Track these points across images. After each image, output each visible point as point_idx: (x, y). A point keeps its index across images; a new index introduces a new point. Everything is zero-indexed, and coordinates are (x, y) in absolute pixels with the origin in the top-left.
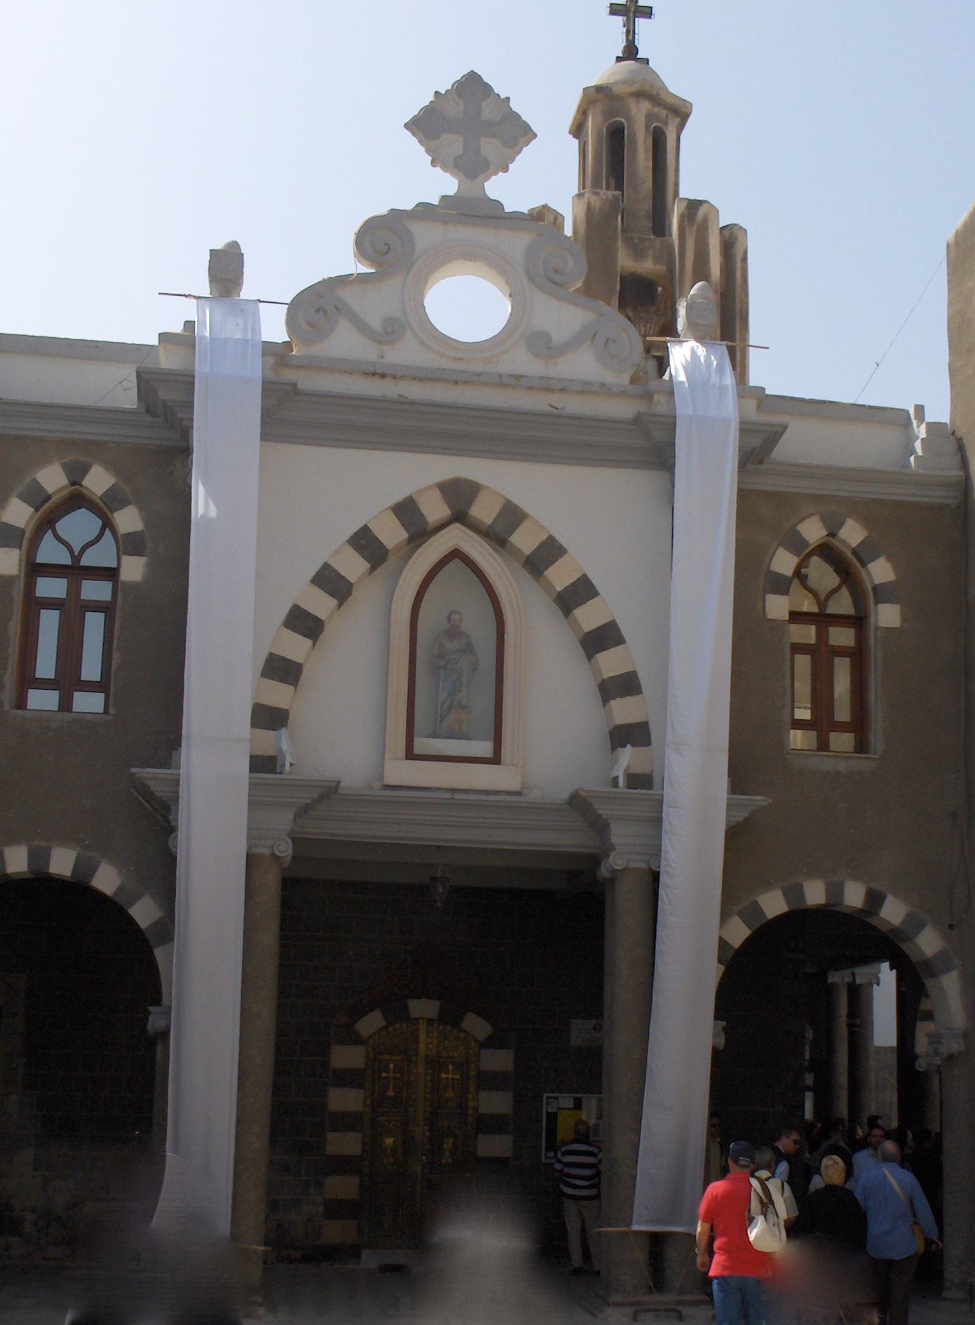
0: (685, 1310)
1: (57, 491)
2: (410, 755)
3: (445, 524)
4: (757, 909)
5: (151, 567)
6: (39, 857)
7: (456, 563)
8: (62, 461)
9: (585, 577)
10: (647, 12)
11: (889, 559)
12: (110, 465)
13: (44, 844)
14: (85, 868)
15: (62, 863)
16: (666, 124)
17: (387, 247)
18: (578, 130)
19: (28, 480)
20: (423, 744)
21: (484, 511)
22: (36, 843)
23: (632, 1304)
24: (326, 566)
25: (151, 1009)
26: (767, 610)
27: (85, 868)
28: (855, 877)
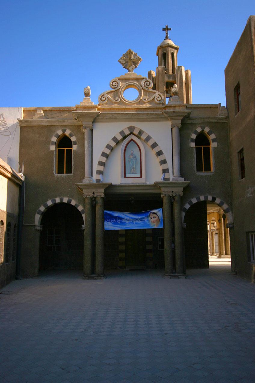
0: (180, 277)
1: (56, 141)
2: (125, 177)
3: (6, 176)
4: (191, 202)
5: (77, 147)
6: (61, 200)
7: (132, 142)
8: (51, 144)
9: (155, 142)
10: (170, 29)
11: (214, 134)
12: (69, 129)
13: (62, 197)
14: (69, 201)
15: (65, 200)
16: (174, 51)
17: (104, 98)
18: (158, 55)
19: (56, 133)
20: (127, 175)
21: (136, 132)
22: (61, 197)
23: (169, 276)
24: (108, 144)
25: (82, 225)
26: (191, 145)
27: (69, 201)
28: (210, 195)
